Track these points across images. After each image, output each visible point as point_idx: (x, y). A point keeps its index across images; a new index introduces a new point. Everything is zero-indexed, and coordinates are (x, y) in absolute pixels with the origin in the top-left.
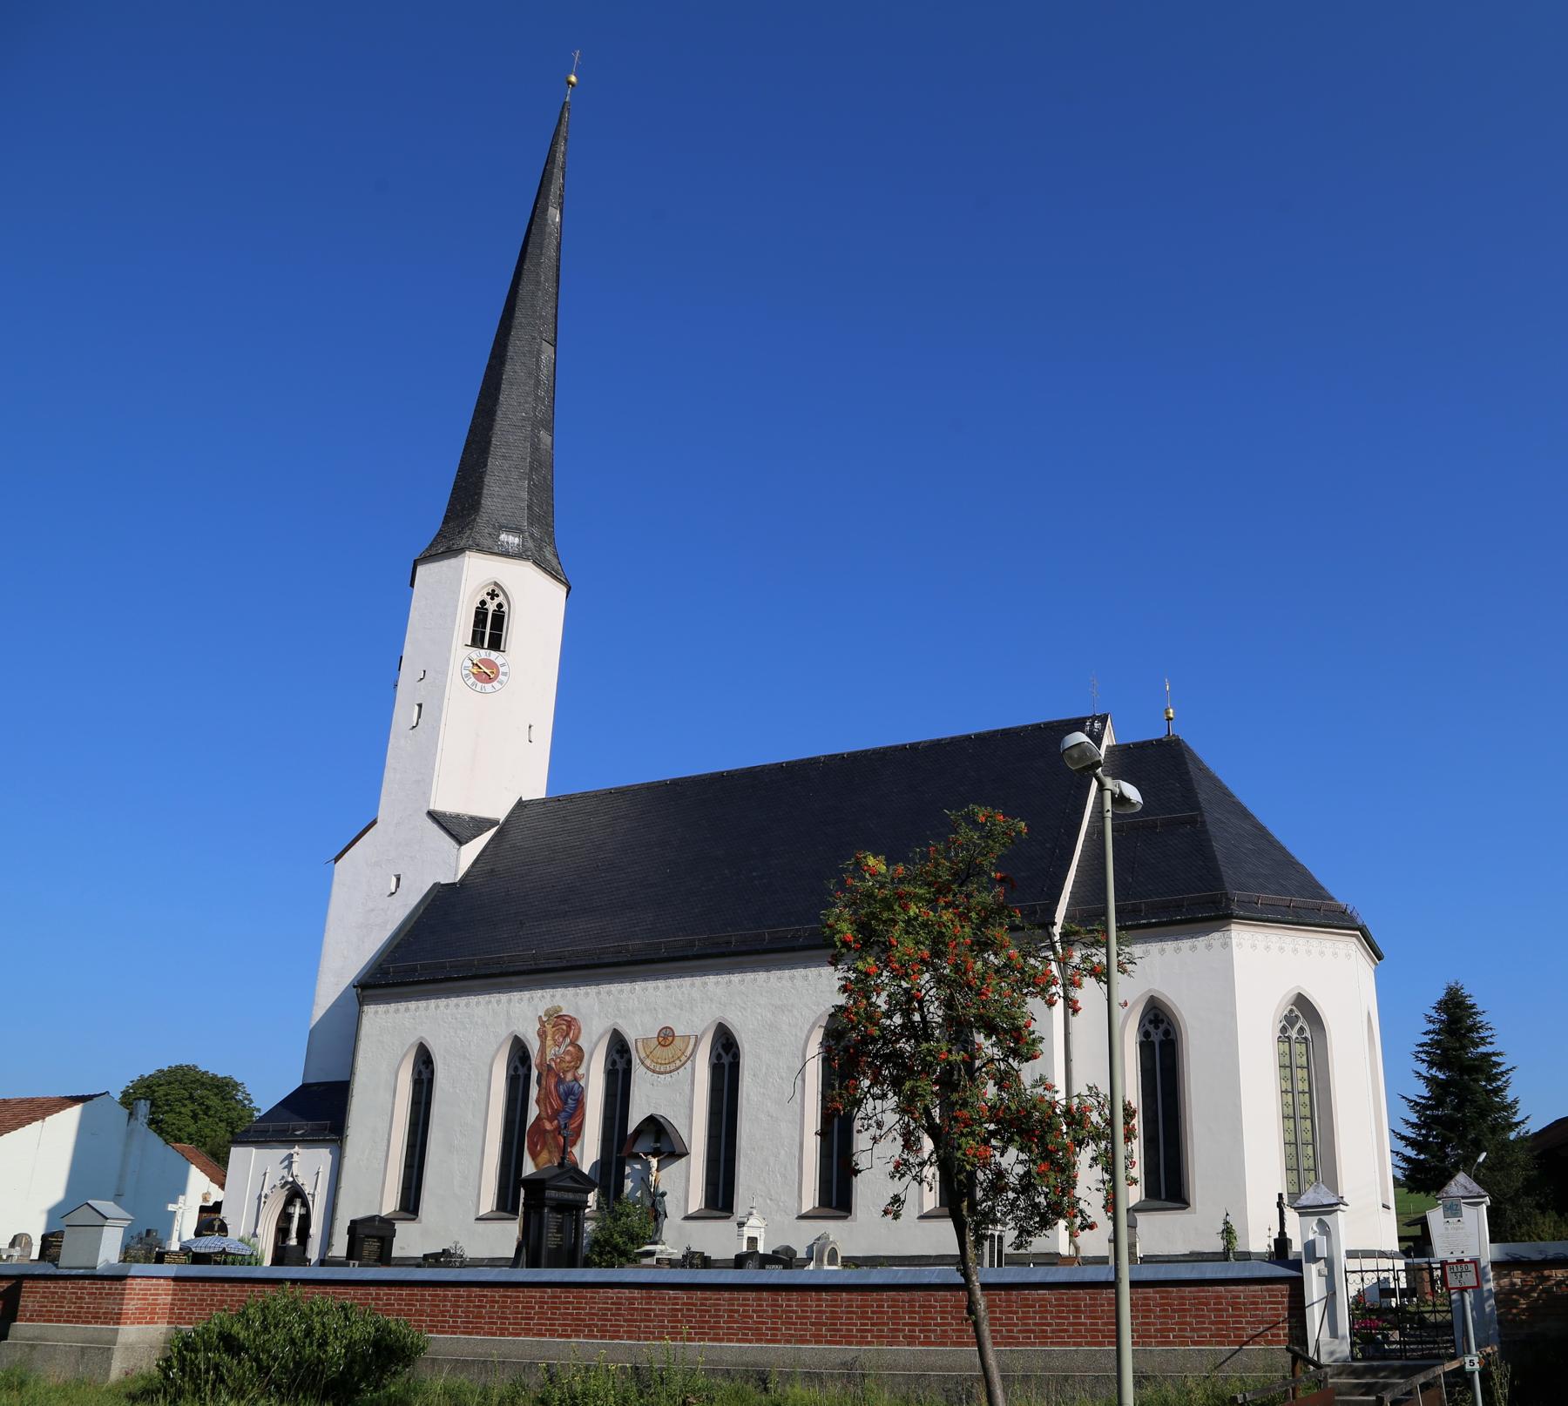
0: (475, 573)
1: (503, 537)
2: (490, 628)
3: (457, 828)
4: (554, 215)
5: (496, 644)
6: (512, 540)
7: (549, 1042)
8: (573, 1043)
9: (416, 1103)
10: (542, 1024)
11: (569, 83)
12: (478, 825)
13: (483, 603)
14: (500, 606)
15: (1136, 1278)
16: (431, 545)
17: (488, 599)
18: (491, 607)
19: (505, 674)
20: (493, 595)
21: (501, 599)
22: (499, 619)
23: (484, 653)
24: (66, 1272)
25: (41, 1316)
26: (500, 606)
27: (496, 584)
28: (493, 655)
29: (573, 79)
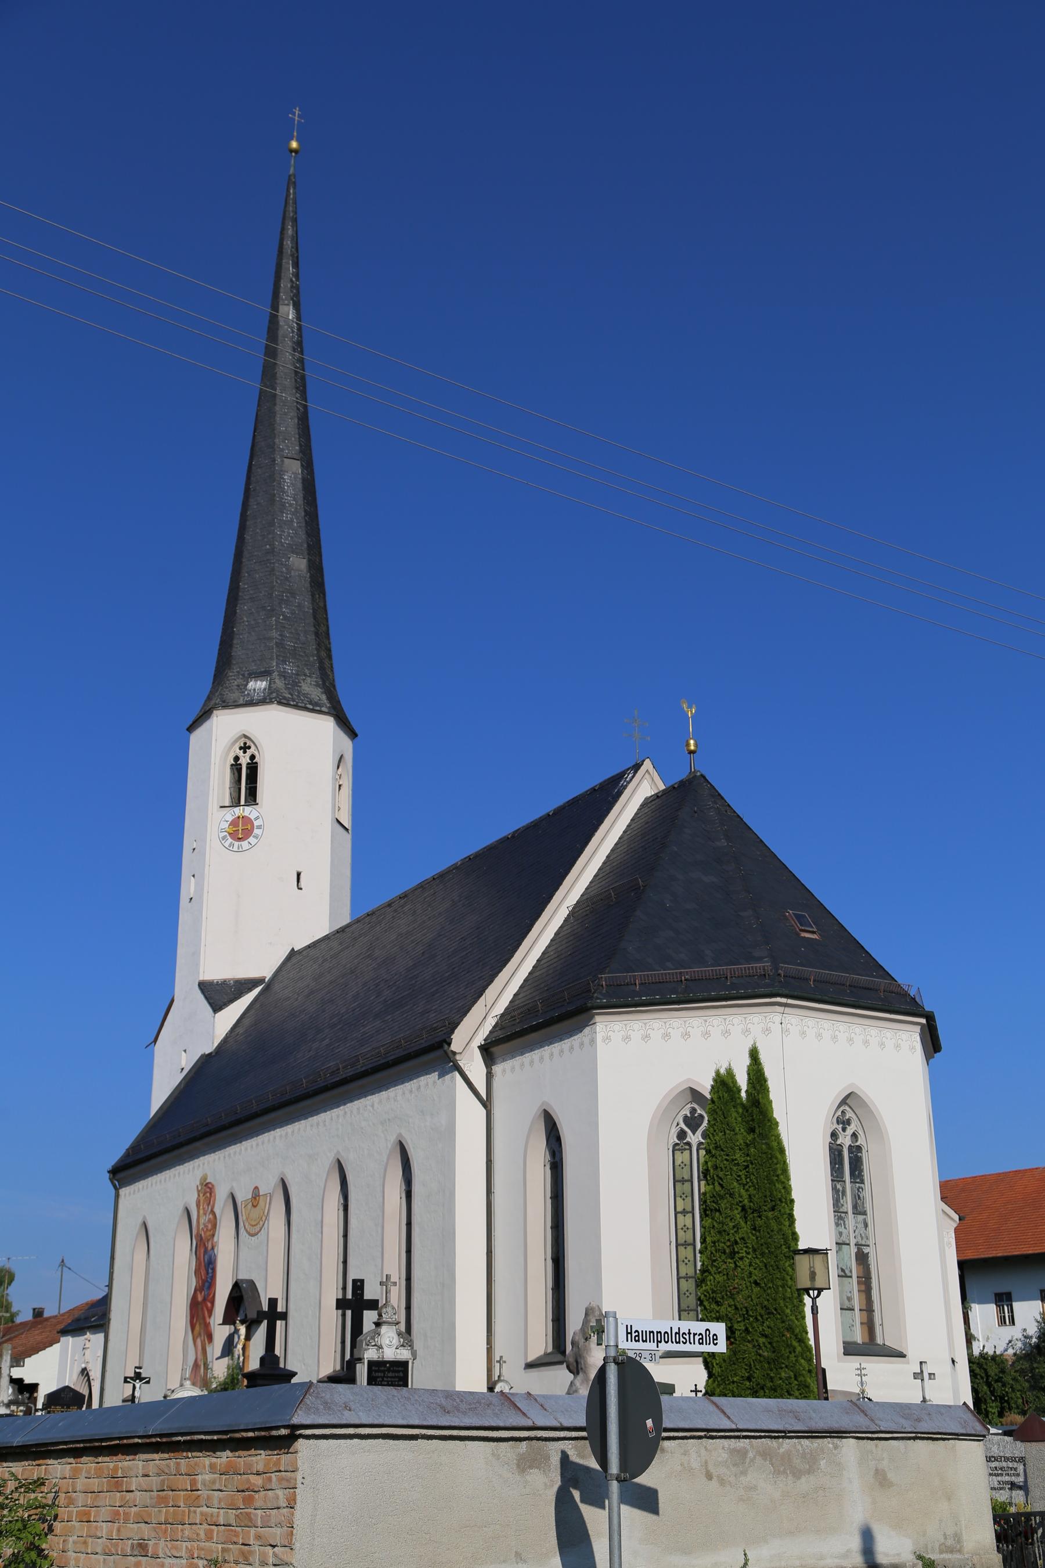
0: (225, 727)
1: (251, 685)
2: (246, 780)
3: (217, 995)
4: (288, 312)
5: (252, 795)
6: (258, 685)
7: (201, 1212)
8: (213, 1212)
9: (985, 1261)
10: (198, 1191)
11: (291, 151)
12: (242, 986)
13: (237, 758)
14: (253, 757)
15: (970, 1255)
16: (204, 705)
17: (241, 753)
18: (244, 760)
19: (259, 827)
20: (245, 748)
21: (252, 750)
22: (253, 769)
23: (238, 811)
24: (615, 1509)
25: (846, 1555)
26: (253, 757)
27: (245, 736)
28: (248, 811)
29: (294, 144)
